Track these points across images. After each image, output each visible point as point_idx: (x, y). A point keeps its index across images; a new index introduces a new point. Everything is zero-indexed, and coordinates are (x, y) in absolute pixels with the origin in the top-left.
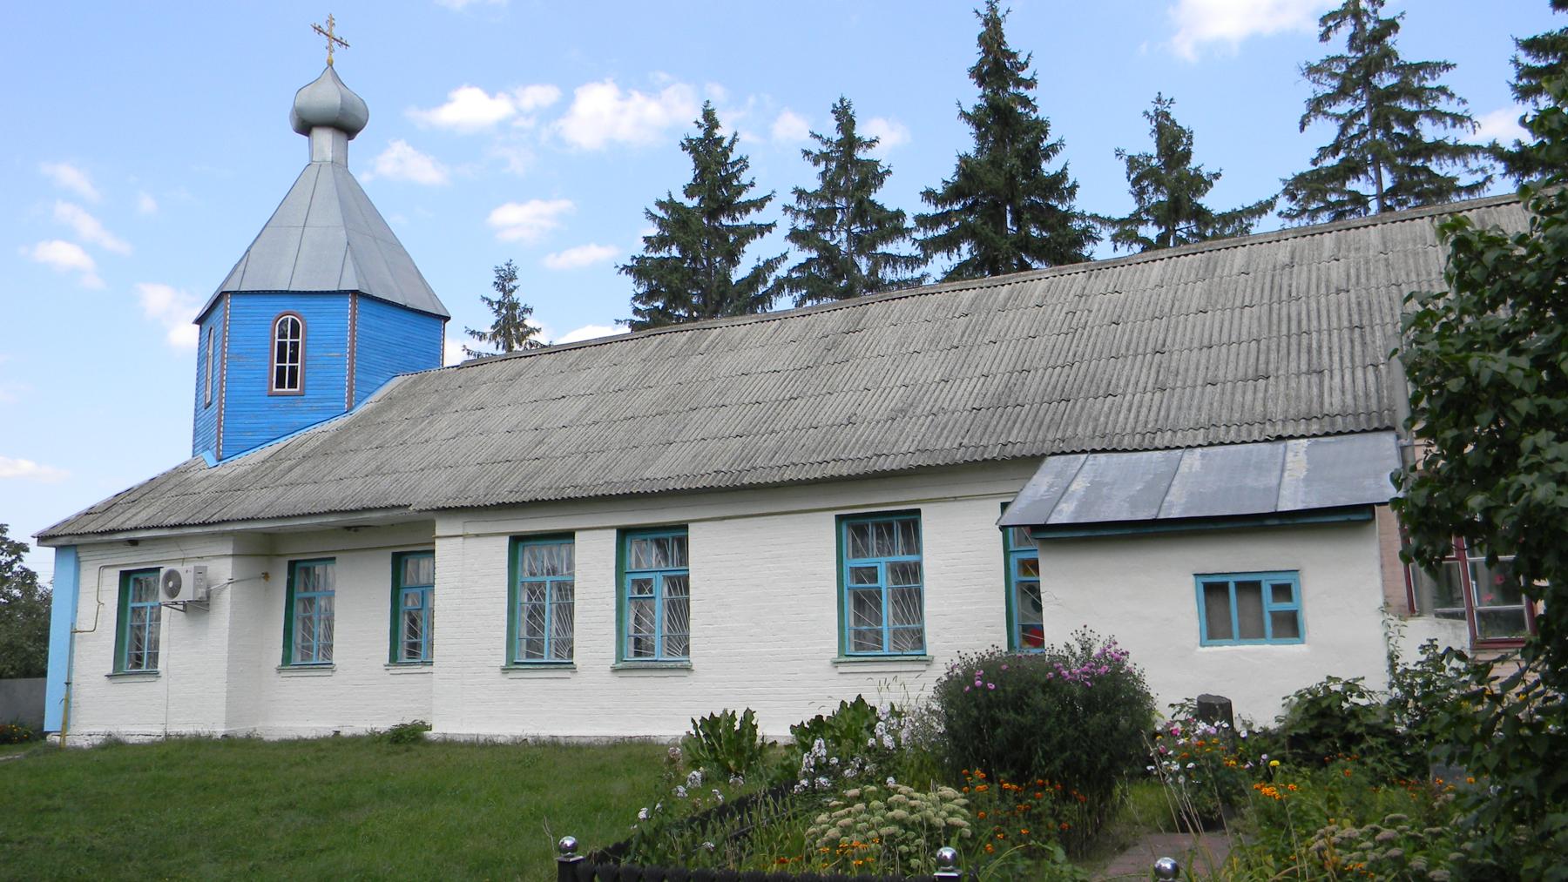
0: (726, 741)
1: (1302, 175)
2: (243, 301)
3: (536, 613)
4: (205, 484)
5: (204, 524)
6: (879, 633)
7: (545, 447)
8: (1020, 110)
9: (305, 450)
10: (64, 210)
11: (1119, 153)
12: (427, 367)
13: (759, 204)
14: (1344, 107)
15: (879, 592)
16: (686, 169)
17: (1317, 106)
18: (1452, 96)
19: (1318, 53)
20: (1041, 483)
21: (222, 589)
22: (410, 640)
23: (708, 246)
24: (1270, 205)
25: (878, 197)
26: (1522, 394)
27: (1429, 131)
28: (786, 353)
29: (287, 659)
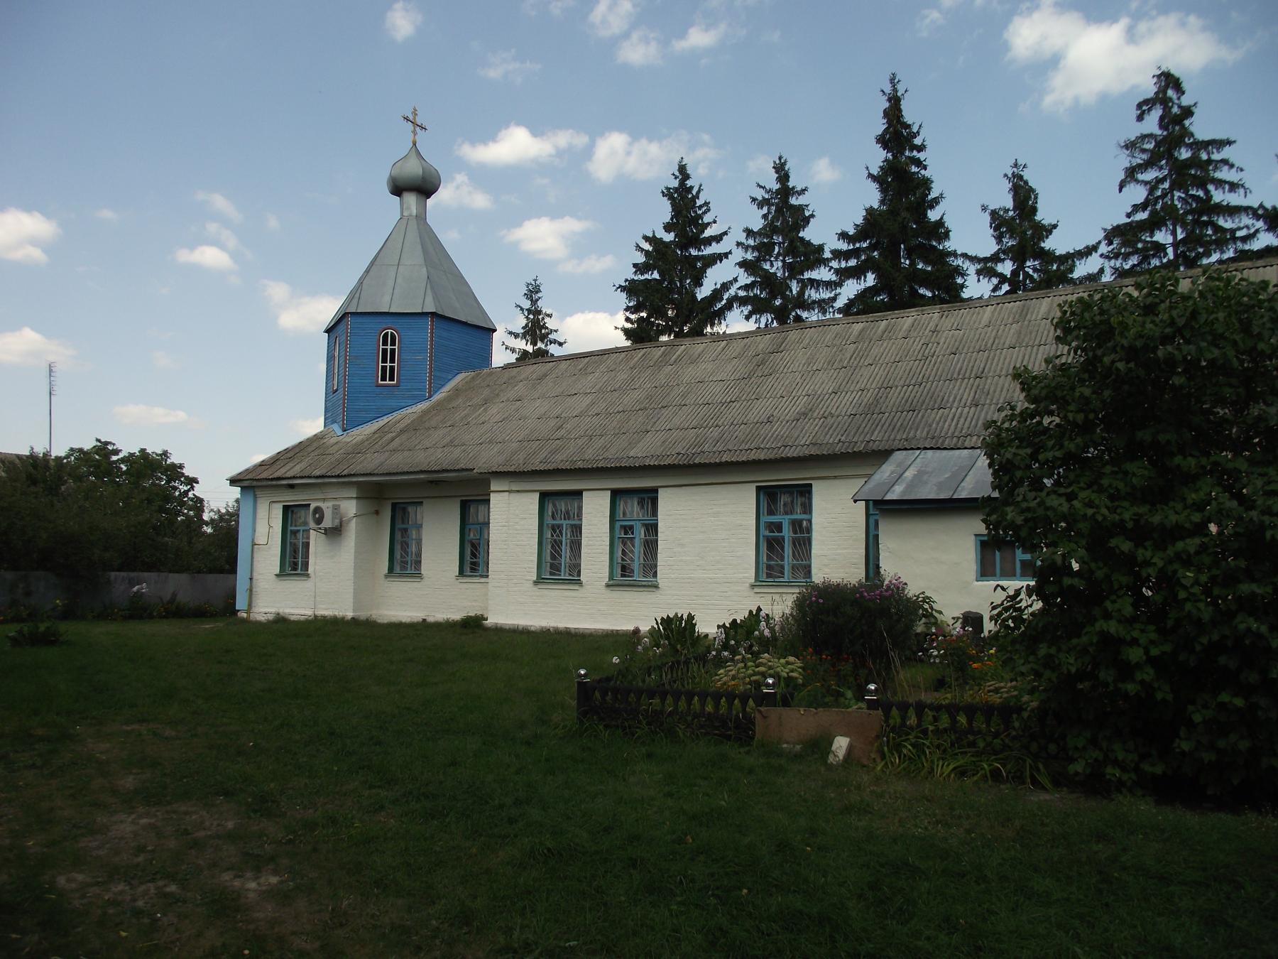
0: (677, 631)
1: (1118, 226)
2: (360, 320)
3: (556, 545)
4: (336, 448)
5: (338, 476)
6: (782, 567)
7: (563, 431)
8: (914, 169)
9: (402, 425)
10: (212, 227)
11: (984, 208)
12: (481, 367)
13: (718, 238)
14: (1150, 175)
15: (783, 538)
16: (665, 211)
17: (1131, 173)
18: (1232, 166)
19: (1134, 130)
20: (886, 471)
21: (350, 520)
22: (473, 560)
23: (681, 271)
24: (1094, 248)
25: (806, 234)
26: (1019, 468)
27: (1218, 196)
28: (729, 367)
29: (391, 570)
